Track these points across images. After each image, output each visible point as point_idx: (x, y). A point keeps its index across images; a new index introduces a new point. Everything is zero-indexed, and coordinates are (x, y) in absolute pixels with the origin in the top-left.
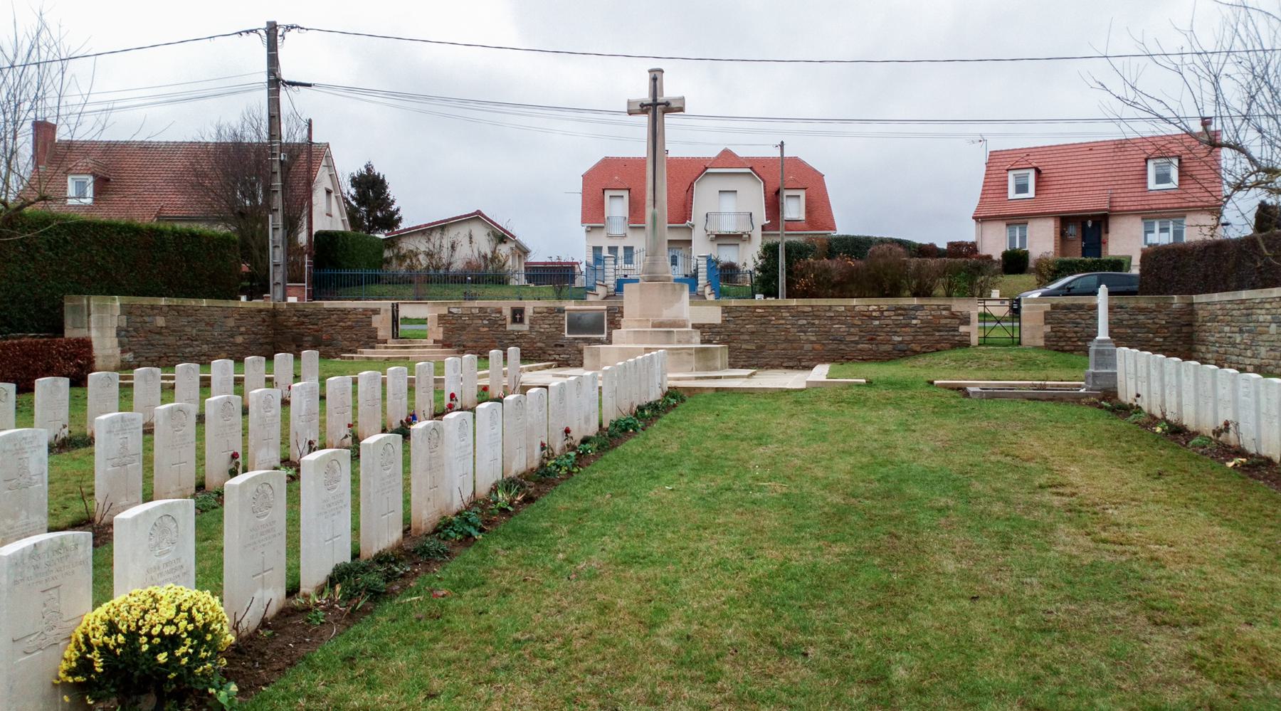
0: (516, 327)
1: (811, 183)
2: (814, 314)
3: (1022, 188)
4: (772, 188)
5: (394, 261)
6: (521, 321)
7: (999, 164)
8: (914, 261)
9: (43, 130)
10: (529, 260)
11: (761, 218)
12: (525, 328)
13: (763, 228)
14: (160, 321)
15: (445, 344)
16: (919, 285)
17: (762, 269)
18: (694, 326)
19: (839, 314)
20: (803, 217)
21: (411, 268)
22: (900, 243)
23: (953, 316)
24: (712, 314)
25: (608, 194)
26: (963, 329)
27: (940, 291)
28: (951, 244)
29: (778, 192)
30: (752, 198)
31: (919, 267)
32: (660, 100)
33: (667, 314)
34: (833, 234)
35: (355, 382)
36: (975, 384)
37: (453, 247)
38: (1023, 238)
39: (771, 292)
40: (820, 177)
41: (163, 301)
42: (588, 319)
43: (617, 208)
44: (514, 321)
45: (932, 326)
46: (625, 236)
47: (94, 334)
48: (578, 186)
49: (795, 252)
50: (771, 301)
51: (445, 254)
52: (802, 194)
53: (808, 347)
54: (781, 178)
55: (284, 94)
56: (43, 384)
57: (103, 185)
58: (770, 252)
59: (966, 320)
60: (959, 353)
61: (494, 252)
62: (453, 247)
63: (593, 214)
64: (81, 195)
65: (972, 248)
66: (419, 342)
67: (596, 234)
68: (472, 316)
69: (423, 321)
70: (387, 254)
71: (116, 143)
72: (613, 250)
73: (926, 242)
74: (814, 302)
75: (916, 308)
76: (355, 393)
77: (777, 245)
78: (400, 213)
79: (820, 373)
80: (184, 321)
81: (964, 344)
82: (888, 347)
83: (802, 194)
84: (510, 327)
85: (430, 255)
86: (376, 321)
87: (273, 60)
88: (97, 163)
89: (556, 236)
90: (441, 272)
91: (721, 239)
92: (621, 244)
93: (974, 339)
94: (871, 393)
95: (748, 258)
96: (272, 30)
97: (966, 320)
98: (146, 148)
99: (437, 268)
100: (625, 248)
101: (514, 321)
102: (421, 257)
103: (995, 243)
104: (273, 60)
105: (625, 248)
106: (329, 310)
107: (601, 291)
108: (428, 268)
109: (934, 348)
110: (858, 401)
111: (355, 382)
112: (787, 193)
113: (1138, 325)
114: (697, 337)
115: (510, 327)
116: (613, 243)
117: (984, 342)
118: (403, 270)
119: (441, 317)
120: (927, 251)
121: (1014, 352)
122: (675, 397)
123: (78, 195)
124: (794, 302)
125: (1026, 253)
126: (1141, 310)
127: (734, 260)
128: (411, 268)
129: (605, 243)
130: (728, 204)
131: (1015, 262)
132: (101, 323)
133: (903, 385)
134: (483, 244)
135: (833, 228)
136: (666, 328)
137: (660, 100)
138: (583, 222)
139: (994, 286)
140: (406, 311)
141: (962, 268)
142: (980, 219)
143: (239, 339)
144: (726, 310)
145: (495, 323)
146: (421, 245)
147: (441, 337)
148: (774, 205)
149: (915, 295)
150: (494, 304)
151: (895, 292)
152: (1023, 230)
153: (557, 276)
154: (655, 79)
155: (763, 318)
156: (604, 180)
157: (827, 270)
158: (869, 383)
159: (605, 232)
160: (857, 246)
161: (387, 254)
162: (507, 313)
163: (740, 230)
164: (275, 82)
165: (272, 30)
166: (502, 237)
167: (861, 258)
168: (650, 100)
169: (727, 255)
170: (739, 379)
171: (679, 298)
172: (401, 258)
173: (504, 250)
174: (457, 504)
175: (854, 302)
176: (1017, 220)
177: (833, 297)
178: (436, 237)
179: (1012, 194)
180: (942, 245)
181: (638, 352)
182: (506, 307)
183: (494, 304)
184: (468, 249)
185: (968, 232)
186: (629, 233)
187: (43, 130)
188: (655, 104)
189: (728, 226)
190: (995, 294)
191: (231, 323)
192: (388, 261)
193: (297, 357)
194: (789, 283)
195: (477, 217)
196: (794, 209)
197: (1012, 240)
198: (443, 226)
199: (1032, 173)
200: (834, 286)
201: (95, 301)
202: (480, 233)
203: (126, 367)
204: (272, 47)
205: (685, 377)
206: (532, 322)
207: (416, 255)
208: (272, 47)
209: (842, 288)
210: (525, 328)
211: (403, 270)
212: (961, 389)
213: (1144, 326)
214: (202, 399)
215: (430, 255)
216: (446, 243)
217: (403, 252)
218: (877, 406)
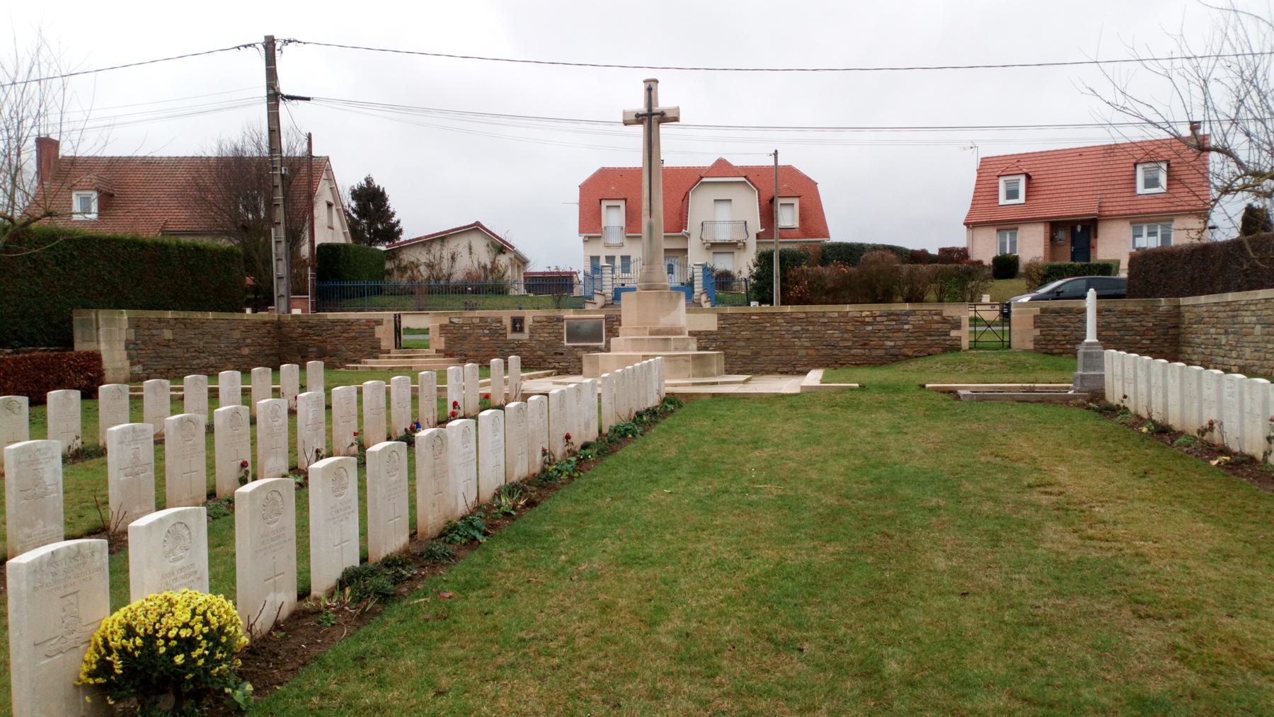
0: (517, 336)
2: (808, 320)
3: (1012, 194)
5: (396, 273)
6: (521, 330)
7: (990, 171)
10: (529, 270)
11: (756, 226)
12: (525, 336)
13: (758, 236)
14: (168, 334)
15: (447, 353)
16: (911, 290)
17: (757, 277)
18: (691, 333)
20: (797, 225)
21: (412, 279)
22: (893, 249)
23: (945, 321)
25: (604, 204)
26: (954, 333)
27: (931, 296)
28: (942, 250)
29: (772, 201)
30: (747, 207)
31: (911, 274)
32: (655, 110)
33: (665, 322)
34: (827, 241)
35: (360, 392)
36: (965, 388)
37: (453, 258)
38: (1013, 244)
39: (766, 299)
40: (811, 186)
41: (170, 314)
42: (586, 327)
43: (614, 218)
44: (514, 330)
45: (924, 331)
47: (103, 348)
49: (789, 260)
50: (766, 308)
51: (445, 265)
52: (796, 202)
53: (802, 352)
54: (777, 186)
55: (284, 107)
57: (107, 201)
58: (765, 259)
59: (957, 325)
60: (950, 357)
61: (493, 263)
62: (453, 258)
63: (590, 224)
65: (963, 254)
68: (473, 326)
69: (425, 331)
72: (610, 259)
74: (808, 308)
76: (360, 402)
77: (771, 253)
78: (401, 225)
81: (955, 348)
82: (881, 352)
83: (796, 202)
84: (510, 336)
85: (430, 266)
87: (272, 75)
89: (553, 244)
90: (442, 282)
91: (717, 247)
92: (618, 254)
93: (965, 344)
94: (865, 398)
95: (743, 265)
97: (957, 325)
99: (438, 279)
100: (623, 257)
101: (514, 330)
102: (422, 268)
103: (986, 249)
104: (272, 75)
105: (623, 257)
107: (599, 300)
108: (428, 279)
110: (851, 405)
111: (360, 392)
113: (1126, 328)
115: (510, 336)
116: (610, 253)
117: (975, 345)
119: (442, 327)
120: (919, 257)
121: (1004, 355)
122: (672, 402)
123: (83, 210)
124: (788, 309)
125: (1017, 258)
127: (729, 268)
128: (412, 279)
129: (603, 253)
130: (723, 213)
131: (1006, 267)
132: (109, 336)
133: (896, 389)
134: (483, 255)
135: (827, 236)
136: (664, 335)
137: (655, 110)
138: (581, 232)
139: (985, 291)
140: (408, 321)
141: (951, 273)
142: (971, 225)
143: (246, 351)
144: (722, 317)
145: (496, 332)
146: (422, 256)
148: (768, 213)
149: (908, 300)
150: (494, 313)
151: (887, 298)
152: (1014, 236)
153: (555, 285)
154: (649, 90)
157: (821, 278)
159: (602, 241)
160: (850, 253)
161: (389, 265)
162: (507, 322)
163: (735, 238)
164: (274, 97)
165: (270, 44)
166: (501, 247)
167: (854, 265)
169: (723, 263)
170: (735, 385)
171: (676, 307)
173: (503, 260)
174: (461, 509)
175: (848, 308)
176: (1006, 225)
178: (436, 248)
179: (1003, 200)
180: (934, 251)
181: (636, 359)
182: (506, 317)
183: (494, 313)
184: (468, 260)
185: (958, 238)
186: (626, 242)
187: (46, 146)
189: (723, 235)
190: (986, 298)
191: (237, 335)
192: (390, 273)
193: (303, 368)
194: (783, 290)
195: (476, 228)
196: (788, 217)
197: (1003, 245)
198: (442, 238)
199: (1023, 179)
200: (828, 293)
201: (103, 315)
202: (479, 244)
203: (136, 379)
205: (682, 383)
206: (532, 331)
207: (417, 266)
209: (835, 295)
210: (525, 336)
211: (404, 281)
212: (952, 392)
215: (430, 266)
216: (446, 254)
217: (404, 264)
218: (869, 409)
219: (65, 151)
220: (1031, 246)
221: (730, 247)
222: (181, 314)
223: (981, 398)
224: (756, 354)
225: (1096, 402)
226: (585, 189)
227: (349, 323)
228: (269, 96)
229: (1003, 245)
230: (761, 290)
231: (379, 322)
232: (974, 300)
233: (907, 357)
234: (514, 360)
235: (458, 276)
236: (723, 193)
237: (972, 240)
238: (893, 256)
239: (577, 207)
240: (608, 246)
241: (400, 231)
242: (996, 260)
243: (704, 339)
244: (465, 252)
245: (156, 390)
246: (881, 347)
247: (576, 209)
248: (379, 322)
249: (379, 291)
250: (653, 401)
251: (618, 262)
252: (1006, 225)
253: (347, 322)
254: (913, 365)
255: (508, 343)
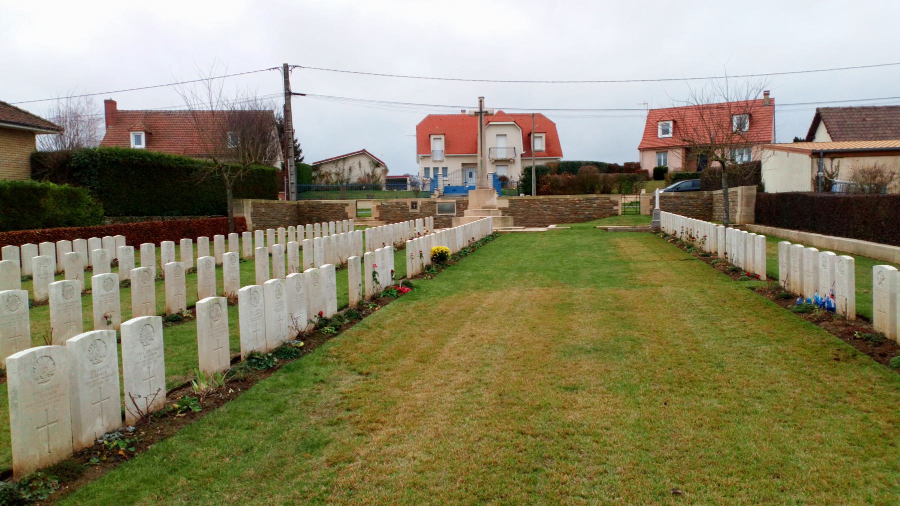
0: (413, 211)
1: (548, 129)
2: (550, 202)
3: (665, 132)
4: (526, 132)
6: (416, 208)
7: (655, 117)
8: (602, 175)
9: (110, 105)
10: (389, 174)
11: (520, 150)
12: (418, 211)
13: (522, 156)
14: (263, 210)
15: (380, 219)
17: (523, 180)
18: (500, 209)
19: (562, 202)
20: (544, 149)
21: (327, 182)
22: (597, 164)
23: (611, 202)
24: (505, 203)
25: (432, 137)
26: (615, 208)
27: (615, 190)
28: (626, 164)
29: (530, 135)
30: (515, 139)
31: (604, 178)
32: (484, 110)
33: (488, 203)
34: (562, 159)
35: (364, 233)
36: (610, 227)
37: (350, 170)
39: (528, 192)
40: (553, 125)
41: (263, 201)
42: (447, 207)
43: (438, 145)
44: (413, 208)
45: (602, 207)
46: (443, 161)
47: (245, 215)
48: (415, 132)
49: (540, 171)
50: (528, 197)
52: (544, 135)
53: (547, 217)
54: (532, 126)
55: (293, 98)
56: (200, 239)
57: (150, 138)
58: (527, 171)
59: (616, 204)
60: (612, 218)
61: (373, 172)
62: (350, 170)
63: (424, 148)
64: (138, 142)
65: (637, 166)
66: (367, 218)
67: (426, 160)
68: (393, 206)
69: (370, 210)
70: (314, 174)
71: (157, 113)
72: (436, 169)
73: (612, 162)
74: (550, 197)
75: (595, 199)
76: (364, 237)
77: (531, 168)
78: (300, 148)
79: (552, 226)
80: (270, 210)
81: (615, 214)
82: (583, 217)
83: (544, 135)
84: (411, 211)
85: (337, 174)
86: (347, 209)
88: (145, 124)
89: (403, 161)
90: (345, 184)
91: (498, 162)
92: (440, 166)
93: (620, 212)
94: (572, 231)
95: (515, 174)
96: (286, 67)
97: (616, 204)
98: (168, 114)
99: (342, 182)
101: (413, 208)
102: (333, 176)
103: (650, 163)
106: (326, 205)
107: (436, 193)
108: (336, 182)
109: (602, 216)
110: (566, 234)
111: (364, 233)
112: (536, 135)
113: (690, 205)
114: (500, 213)
115: (411, 211)
116: (436, 165)
117: (624, 213)
118: (323, 183)
120: (612, 168)
121: (637, 217)
122: (495, 235)
123: (137, 143)
124: (541, 197)
125: (667, 168)
126: (691, 198)
127: (505, 174)
128: (327, 182)
129: (431, 166)
130: (502, 142)
131: (660, 173)
132: (246, 209)
134: (367, 168)
135: (561, 155)
136: (488, 209)
137: (484, 110)
138: (418, 153)
139: (642, 187)
140: (362, 205)
141: (628, 176)
142: (642, 149)
143: (287, 218)
144: (511, 201)
145: (404, 209)
146: (332, 169)
147: (378, 216)
149: (603, 193)
151: (592, 192)
152: (665, 156)
153: (399, 183)
155: (527, 205)
156: (429, 129)
157: (557, 181)
158: (572, 228)
159: (431, 159)
160: (573, 167)
161: (314, 174)
162: (409, 204)
163: (509, 157)
164: (288, 94)
165: (286, 67)
166: (377, 164)
168: (478, 110)
169: (502, 172)
170: (520, 229)
171: (493, 196)
172: (322, 176)
173: (379, 171)
174: (458, 249)
175: (568, 197)
176: (661, 150)
177: (560, 194)
178: (340, 164)
179: (660, 135)
180: (621, 164)
181: (476, 219)
182: (409, 202)
184: (358, 171)
185: (634, 157)
186: (445, 159)
187: (110, 105)
188: (481, 112)
189: (501, 155)
190: (643, 191)
191: (284, 211)
192: (314, 178)
194: (538, 188)
195: (363, 153)
196: (539, 144)
197: (659, 161)
198: (344, 158)
199: (671, 123)
200: (561, 189)
202: (365, 162)
203: (254, 229)
204: (286, 76)
205: (499, 228)
206: (421, 208)
207: (330, 174)
208: (286, 76)
209: (564, 190)
210: (418, 211)
211: (323, 183)
212: (606, 229)
213: (692, 205)
214: (287, 242)
216: (347, 167)
218: (573, 234)
219: (119, 107)
220: (675, 162)
221: (506, 162)
222: (267, 201)
223: (616, 231)
224: (527, 218)
225: (657, 230)
226: (420, 128)
227: (332, 205)
228: (286, 94)
229: (659, 161)
230: (525, 186)
231: (347, 205)
232: (637, 192)
233: (595, 219)
234: (430, 220)
235: (354, 180)
236: (501, 131)
237: (642, 158)
238: (596, 168)
239: (415, 139)
240: (434, 162)
241: (301, 151)
242: (655, 170)
243: (504, 211)
244: (357, 167)
245: (259, 233)
246: (583, 214)
247: (415, 140)
248: (347, 205)
249: (310, 189)
250: (490, 233)
251: (440, 172)
252: (661, 150)
253: (332, 205)
254: (596, 221)
255: (409, 214)
